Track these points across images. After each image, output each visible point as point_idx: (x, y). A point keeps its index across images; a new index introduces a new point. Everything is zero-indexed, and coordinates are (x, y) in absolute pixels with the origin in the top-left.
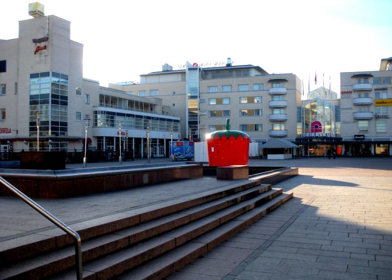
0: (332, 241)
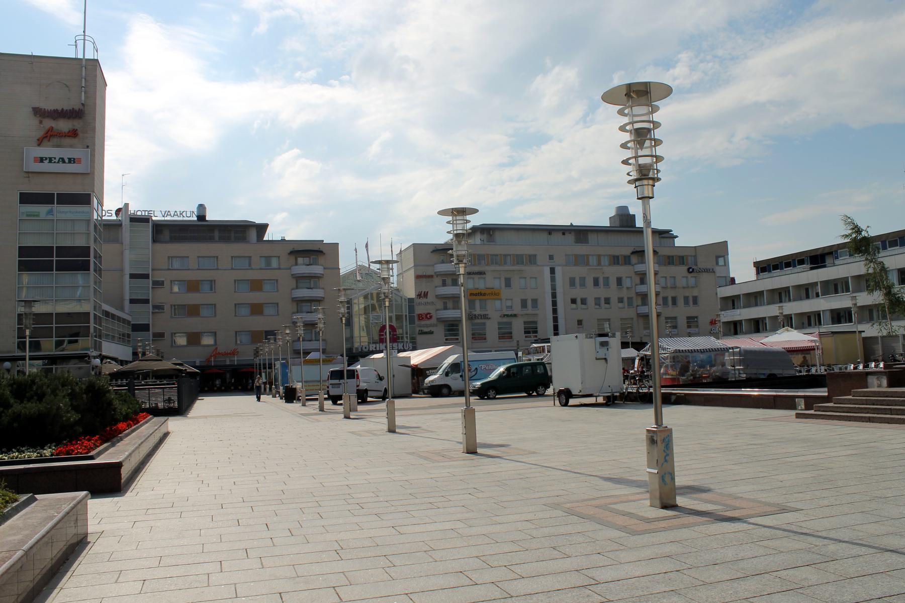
0: (208, 574)
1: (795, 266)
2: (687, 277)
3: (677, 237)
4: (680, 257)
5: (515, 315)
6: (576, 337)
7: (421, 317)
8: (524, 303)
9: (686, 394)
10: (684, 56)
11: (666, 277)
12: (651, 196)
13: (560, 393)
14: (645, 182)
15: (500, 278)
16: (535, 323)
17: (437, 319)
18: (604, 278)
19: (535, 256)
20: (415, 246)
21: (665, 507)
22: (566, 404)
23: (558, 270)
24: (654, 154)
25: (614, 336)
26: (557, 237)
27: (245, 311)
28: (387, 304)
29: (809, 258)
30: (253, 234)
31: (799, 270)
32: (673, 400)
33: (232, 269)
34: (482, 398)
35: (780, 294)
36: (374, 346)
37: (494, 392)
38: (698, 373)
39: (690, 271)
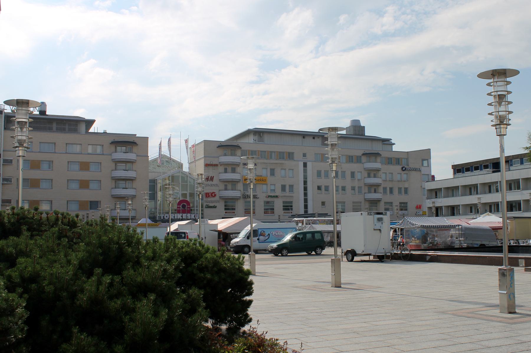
1: (481, 170)
2: (401, 174)
3: (394, 144)
4: (396, 159)
5: (277, 197)
6: (362, 214)
7: (208, 195)
8: (283, 188)
9: (438, 255)
10: (391, 9)
11: (386, 173)
12: (505, 134)
13: (347, 253)
14: (502, 126)
15: (267, 169)
16: (291, 202)
17: (220, 197)
18: (342, 172)
19: (293, 153)
20: (206, 142)
21: (510, 313)
22: (352, 260)
23: (309, 165)
24: (507, 110)
25: (386, 214)
26: (309, 140)
27: (75, 185)
28: (252, 187)
29: (492, 164)
30: (83, 127)
31: (485, 172)
32: (427, 259)
33: (66, 153)
34: (276, 255)
35: (470, 189)
36: (173, 215)
37: (286, 251)
38: (435, 242)
39: (404, 169)
